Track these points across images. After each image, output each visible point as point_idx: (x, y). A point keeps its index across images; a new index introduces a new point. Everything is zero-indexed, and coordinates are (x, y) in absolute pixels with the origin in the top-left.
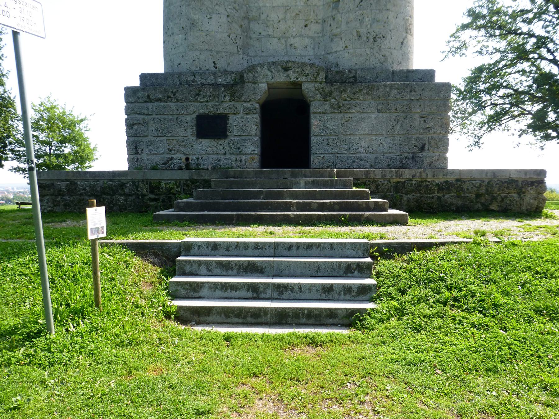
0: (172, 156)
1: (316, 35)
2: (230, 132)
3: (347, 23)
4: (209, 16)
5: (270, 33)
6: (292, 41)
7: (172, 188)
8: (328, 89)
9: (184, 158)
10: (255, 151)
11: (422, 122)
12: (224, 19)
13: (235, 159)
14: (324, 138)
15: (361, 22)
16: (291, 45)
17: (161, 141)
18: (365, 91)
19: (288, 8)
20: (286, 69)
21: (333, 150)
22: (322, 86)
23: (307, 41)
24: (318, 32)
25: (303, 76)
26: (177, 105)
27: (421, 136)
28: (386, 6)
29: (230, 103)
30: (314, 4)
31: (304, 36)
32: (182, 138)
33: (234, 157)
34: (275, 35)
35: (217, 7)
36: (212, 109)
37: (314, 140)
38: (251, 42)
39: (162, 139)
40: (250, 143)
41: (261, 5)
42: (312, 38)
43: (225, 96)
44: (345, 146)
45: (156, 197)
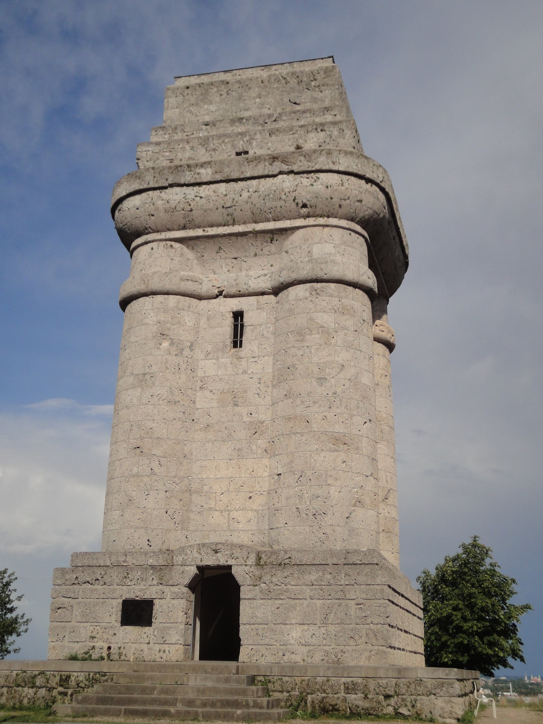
0: (95, 644)
1: (260, 508)
2: (156, 619)
3: (287, 499)
4: (146, 493)
5: (212, 506)
6: (234, 514)
7: (82, 682)
8: (257, 573)
9: (106, 646)
10: (179, 640)
11: (358, 611)
12: (162, 495)
13: (158, 649)
14: (253, 626)
15: (301, 497)
16: (233, 519)
17: (85, 627)
18: (297, 575)
19: (232, 479)
20: (216, 552)
21: (262, 641)
22: (251, 570)
23: (250, 514)
24: (262, 505)
25: (233, 559)
26: (104, 589)
27: (358, 626)
28: (326, 481)
29: (158, 587)
30: (259, 475)
31: (248, 509)
32: (106, 624)
33: (157, 647)
34: (217, 508)
35: (155, 484)
36: (139, 593)
37: (243, 629)
38: (192, 515)
39: (85, 624)
40: (175, 632)
41: (204, 477)
42: (256, 510)
43: (153, 579)
44: (275, 636)
45: (66, 690)
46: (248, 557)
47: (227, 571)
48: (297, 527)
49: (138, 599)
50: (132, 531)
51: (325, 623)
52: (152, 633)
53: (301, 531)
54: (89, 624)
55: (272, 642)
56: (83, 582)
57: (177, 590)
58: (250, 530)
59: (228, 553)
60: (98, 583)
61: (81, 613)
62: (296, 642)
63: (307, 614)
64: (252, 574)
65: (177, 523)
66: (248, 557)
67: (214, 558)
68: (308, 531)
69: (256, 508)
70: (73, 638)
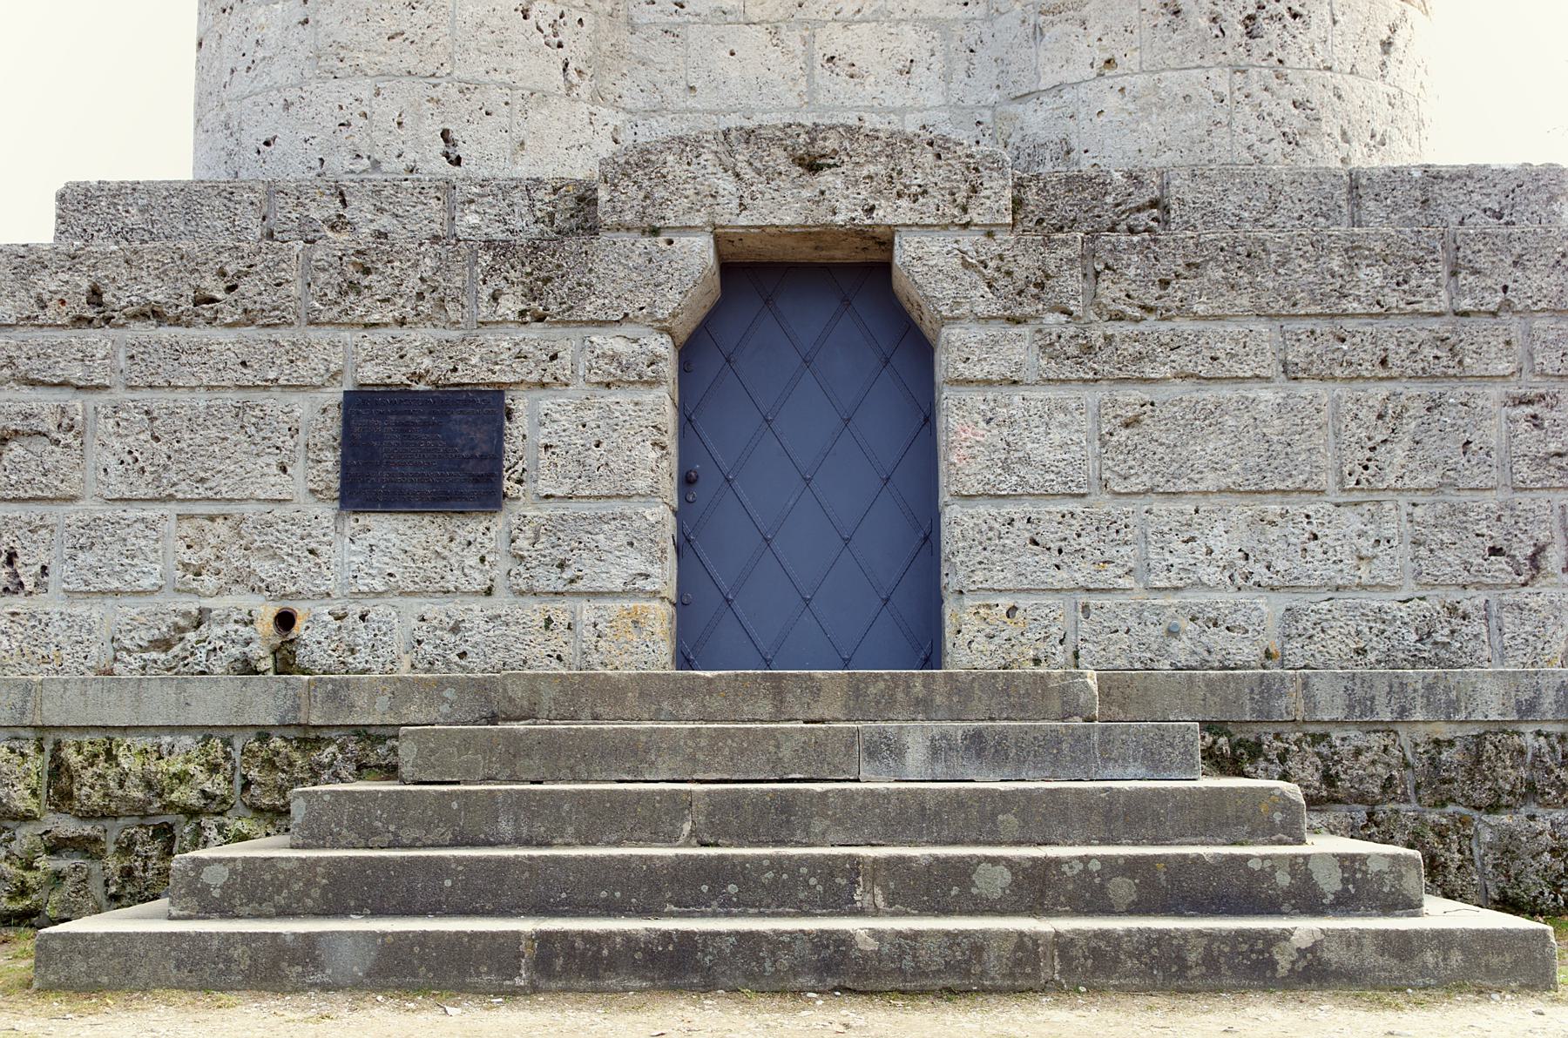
0: (206, 603)
2: (520, 482)
6: (836, 40)
9: (267, 612)
14: (1009, 509)
21: (1063, 574)
23: (910, 41)
27: (1525, 499)
29: (522, 333)
36: (427, 362)
39: (152, 512)
40: (621, 538)
46: (974, 190)
47: (876, 256)
48: (1169, 74)
49: (421, 387)
50: (364, 89)
51: (1364, 484)
52: (504, 547)
53: (1190, 91)
54: (172, 509)
55: (1109, 575)
56: (129, 310)
57: (620, 346)
58: (913, 109)
59: (872, 169)
60: (208, 314)
61: (129, 459)
62: (1227, 574)
63: (1279, 447)
64: (998, 269)
65: (572, 66)
66: (974, 190)
67: (806, 193)
68: (1227, 92)
69: (936, 12)
70: (90, 576)
